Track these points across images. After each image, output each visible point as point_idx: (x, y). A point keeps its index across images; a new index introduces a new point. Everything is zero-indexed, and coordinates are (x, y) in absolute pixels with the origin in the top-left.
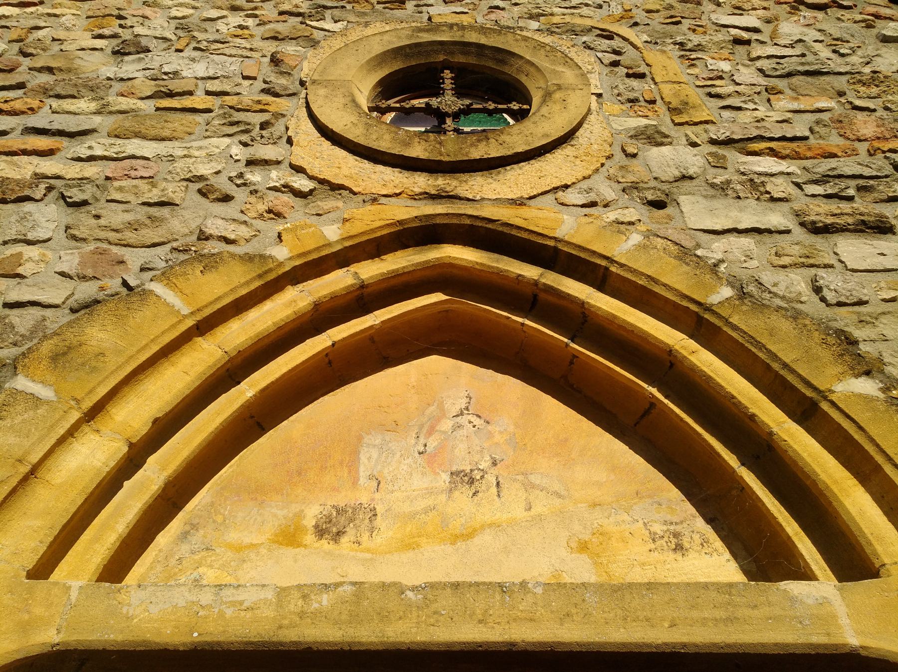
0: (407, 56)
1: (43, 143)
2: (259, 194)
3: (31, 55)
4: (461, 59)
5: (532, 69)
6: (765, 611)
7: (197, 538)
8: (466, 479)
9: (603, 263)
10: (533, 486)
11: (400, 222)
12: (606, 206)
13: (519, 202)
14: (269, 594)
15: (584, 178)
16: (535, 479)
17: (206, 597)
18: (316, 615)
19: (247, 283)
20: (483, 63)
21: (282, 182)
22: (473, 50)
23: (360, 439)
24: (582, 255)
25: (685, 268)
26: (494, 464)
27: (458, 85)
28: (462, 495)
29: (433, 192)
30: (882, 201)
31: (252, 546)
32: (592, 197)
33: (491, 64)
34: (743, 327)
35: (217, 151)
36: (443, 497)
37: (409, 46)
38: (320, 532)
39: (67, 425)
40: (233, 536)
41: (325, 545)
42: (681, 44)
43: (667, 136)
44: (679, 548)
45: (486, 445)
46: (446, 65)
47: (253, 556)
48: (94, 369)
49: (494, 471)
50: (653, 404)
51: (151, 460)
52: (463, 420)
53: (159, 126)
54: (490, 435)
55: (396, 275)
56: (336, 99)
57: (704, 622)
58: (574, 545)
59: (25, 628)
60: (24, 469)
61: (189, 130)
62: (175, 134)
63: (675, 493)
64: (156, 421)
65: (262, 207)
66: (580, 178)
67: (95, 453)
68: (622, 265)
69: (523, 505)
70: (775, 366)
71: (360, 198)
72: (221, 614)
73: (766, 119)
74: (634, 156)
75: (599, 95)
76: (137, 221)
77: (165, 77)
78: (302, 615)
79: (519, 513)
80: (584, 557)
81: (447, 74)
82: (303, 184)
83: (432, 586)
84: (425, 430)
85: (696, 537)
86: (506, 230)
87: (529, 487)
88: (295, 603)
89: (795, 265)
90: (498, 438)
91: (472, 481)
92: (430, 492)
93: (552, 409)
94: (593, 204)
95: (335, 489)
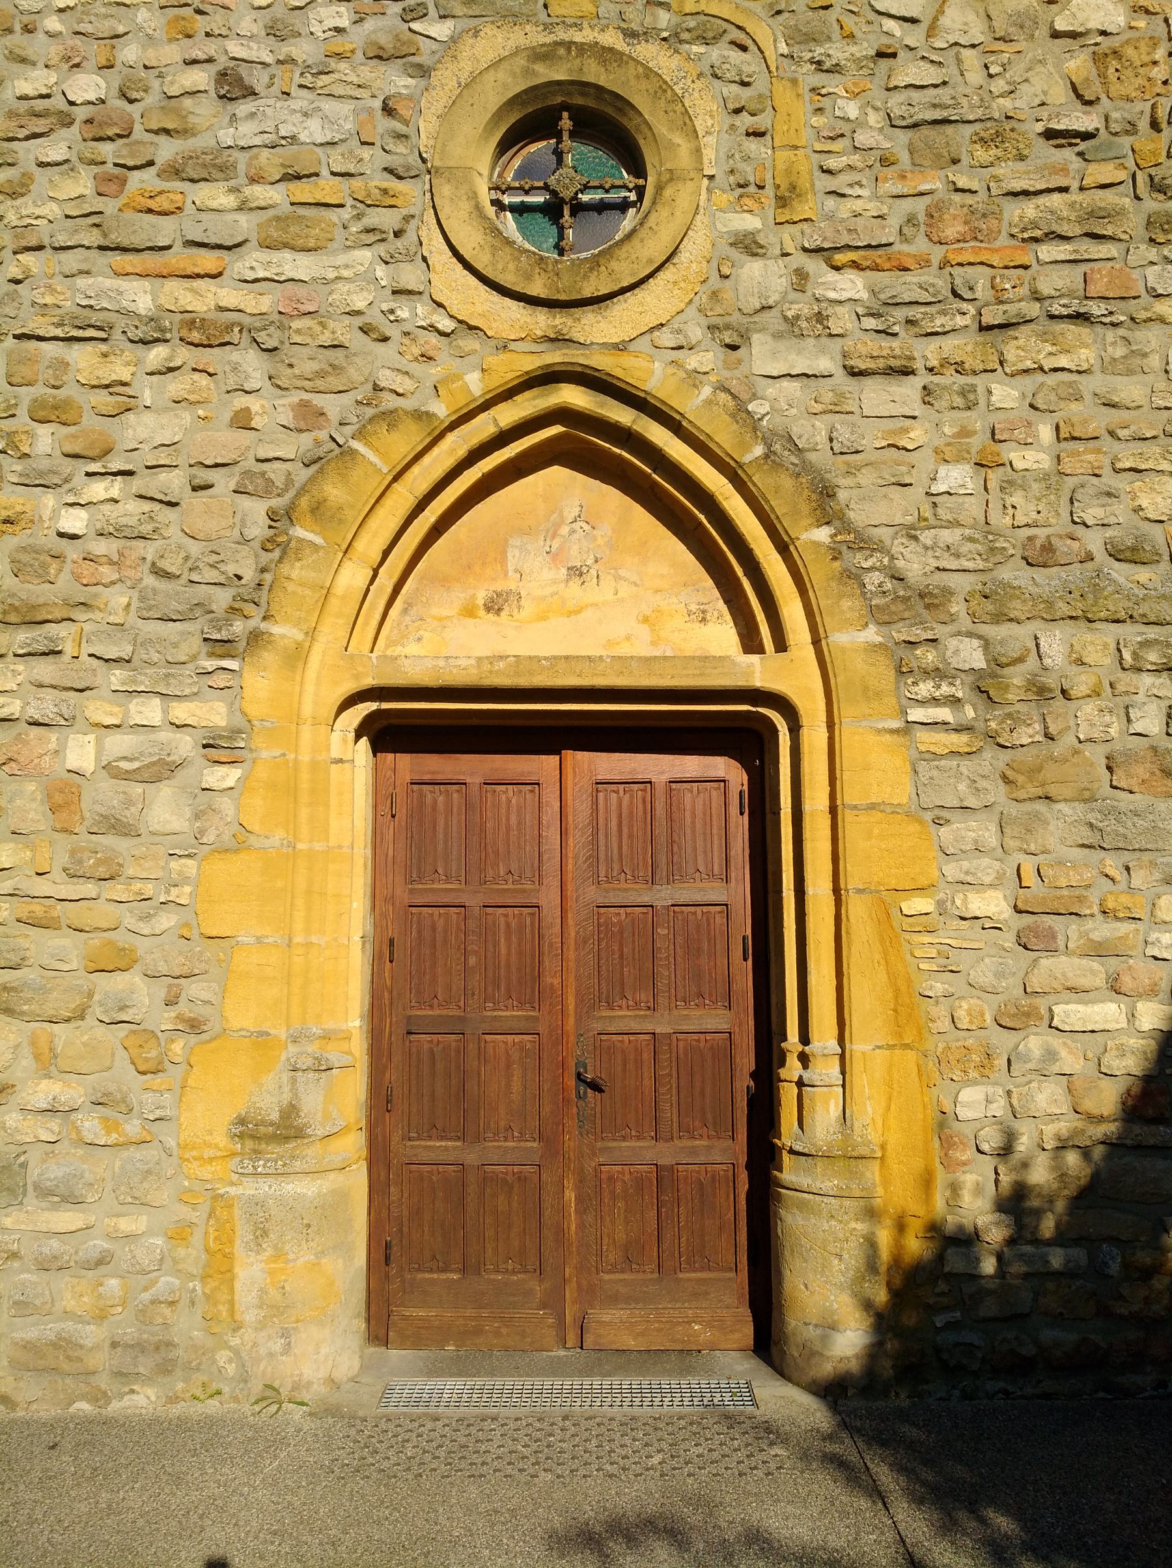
0: (524, 104)
1: (208, 261)
2: (412, 336)
3: (136, 100)
4: (579, 101)
5: (649, 134)
6: (720, 670)
7: (413, 612)
8: (577, 572)
9: (678, 417)
10: (620, 578)
13: (620, 347)
14: (473, 662)
16: (622, 572)
17: (442, 663)
18: (497, 672)
19: (422, 441)
20: (602, 108)
21: (428, 321)
22: (592, 91)
23: (506, 541)
24: (664, 408)
25: (735, 427)
26: (596, 561)
27: (579, 137)
28: (575, 583)
29: (552, 336)
31: (448, 618)
32: (681, 340)
33: (609, 110)
34: (760, 485)
35: (363, 269)
36: (563, 585)
37: (525, 92)
38: (488, 609)
40: (435, 611)
41: (491, 616)
42: (819, 63)
43: (762, 247)
44: (704, 620)
45: (591, 546)
46: (565, 107)
47: (449, 623)
48: (340, 521)
49: (596, 566)
50: (701, 524)
52: (576, 526)
54: (595, 539)
56: (461, 204)
57: (688, 676)
58: (640, 618)
61: (329, 236)
62: (319, 244)
63: (710, 583)
65: (416, 351)
68: (691, 422)
69: (612, 591)
70: (773, 516)
71: (493, 343)
72: (451, 672)
73: (864, 213)
74: (727, 277)
75: (711, 178)
76: (322, 370)
77: (283, 142)
78: (491, 672)
79: (610, 597)
80: (646, 626)
81: (565, 115)
82: (446, 324)
83: (555, 658)
84: (550, 534)
85: (716, 613)
86: (609, 379)
87: (618, 578)
88: (486, 667)
90: (600, 541)
91: (581, 575)
92: (554, 582)
93: (639, 512)
94: (680, 348)
95: (494, 579)
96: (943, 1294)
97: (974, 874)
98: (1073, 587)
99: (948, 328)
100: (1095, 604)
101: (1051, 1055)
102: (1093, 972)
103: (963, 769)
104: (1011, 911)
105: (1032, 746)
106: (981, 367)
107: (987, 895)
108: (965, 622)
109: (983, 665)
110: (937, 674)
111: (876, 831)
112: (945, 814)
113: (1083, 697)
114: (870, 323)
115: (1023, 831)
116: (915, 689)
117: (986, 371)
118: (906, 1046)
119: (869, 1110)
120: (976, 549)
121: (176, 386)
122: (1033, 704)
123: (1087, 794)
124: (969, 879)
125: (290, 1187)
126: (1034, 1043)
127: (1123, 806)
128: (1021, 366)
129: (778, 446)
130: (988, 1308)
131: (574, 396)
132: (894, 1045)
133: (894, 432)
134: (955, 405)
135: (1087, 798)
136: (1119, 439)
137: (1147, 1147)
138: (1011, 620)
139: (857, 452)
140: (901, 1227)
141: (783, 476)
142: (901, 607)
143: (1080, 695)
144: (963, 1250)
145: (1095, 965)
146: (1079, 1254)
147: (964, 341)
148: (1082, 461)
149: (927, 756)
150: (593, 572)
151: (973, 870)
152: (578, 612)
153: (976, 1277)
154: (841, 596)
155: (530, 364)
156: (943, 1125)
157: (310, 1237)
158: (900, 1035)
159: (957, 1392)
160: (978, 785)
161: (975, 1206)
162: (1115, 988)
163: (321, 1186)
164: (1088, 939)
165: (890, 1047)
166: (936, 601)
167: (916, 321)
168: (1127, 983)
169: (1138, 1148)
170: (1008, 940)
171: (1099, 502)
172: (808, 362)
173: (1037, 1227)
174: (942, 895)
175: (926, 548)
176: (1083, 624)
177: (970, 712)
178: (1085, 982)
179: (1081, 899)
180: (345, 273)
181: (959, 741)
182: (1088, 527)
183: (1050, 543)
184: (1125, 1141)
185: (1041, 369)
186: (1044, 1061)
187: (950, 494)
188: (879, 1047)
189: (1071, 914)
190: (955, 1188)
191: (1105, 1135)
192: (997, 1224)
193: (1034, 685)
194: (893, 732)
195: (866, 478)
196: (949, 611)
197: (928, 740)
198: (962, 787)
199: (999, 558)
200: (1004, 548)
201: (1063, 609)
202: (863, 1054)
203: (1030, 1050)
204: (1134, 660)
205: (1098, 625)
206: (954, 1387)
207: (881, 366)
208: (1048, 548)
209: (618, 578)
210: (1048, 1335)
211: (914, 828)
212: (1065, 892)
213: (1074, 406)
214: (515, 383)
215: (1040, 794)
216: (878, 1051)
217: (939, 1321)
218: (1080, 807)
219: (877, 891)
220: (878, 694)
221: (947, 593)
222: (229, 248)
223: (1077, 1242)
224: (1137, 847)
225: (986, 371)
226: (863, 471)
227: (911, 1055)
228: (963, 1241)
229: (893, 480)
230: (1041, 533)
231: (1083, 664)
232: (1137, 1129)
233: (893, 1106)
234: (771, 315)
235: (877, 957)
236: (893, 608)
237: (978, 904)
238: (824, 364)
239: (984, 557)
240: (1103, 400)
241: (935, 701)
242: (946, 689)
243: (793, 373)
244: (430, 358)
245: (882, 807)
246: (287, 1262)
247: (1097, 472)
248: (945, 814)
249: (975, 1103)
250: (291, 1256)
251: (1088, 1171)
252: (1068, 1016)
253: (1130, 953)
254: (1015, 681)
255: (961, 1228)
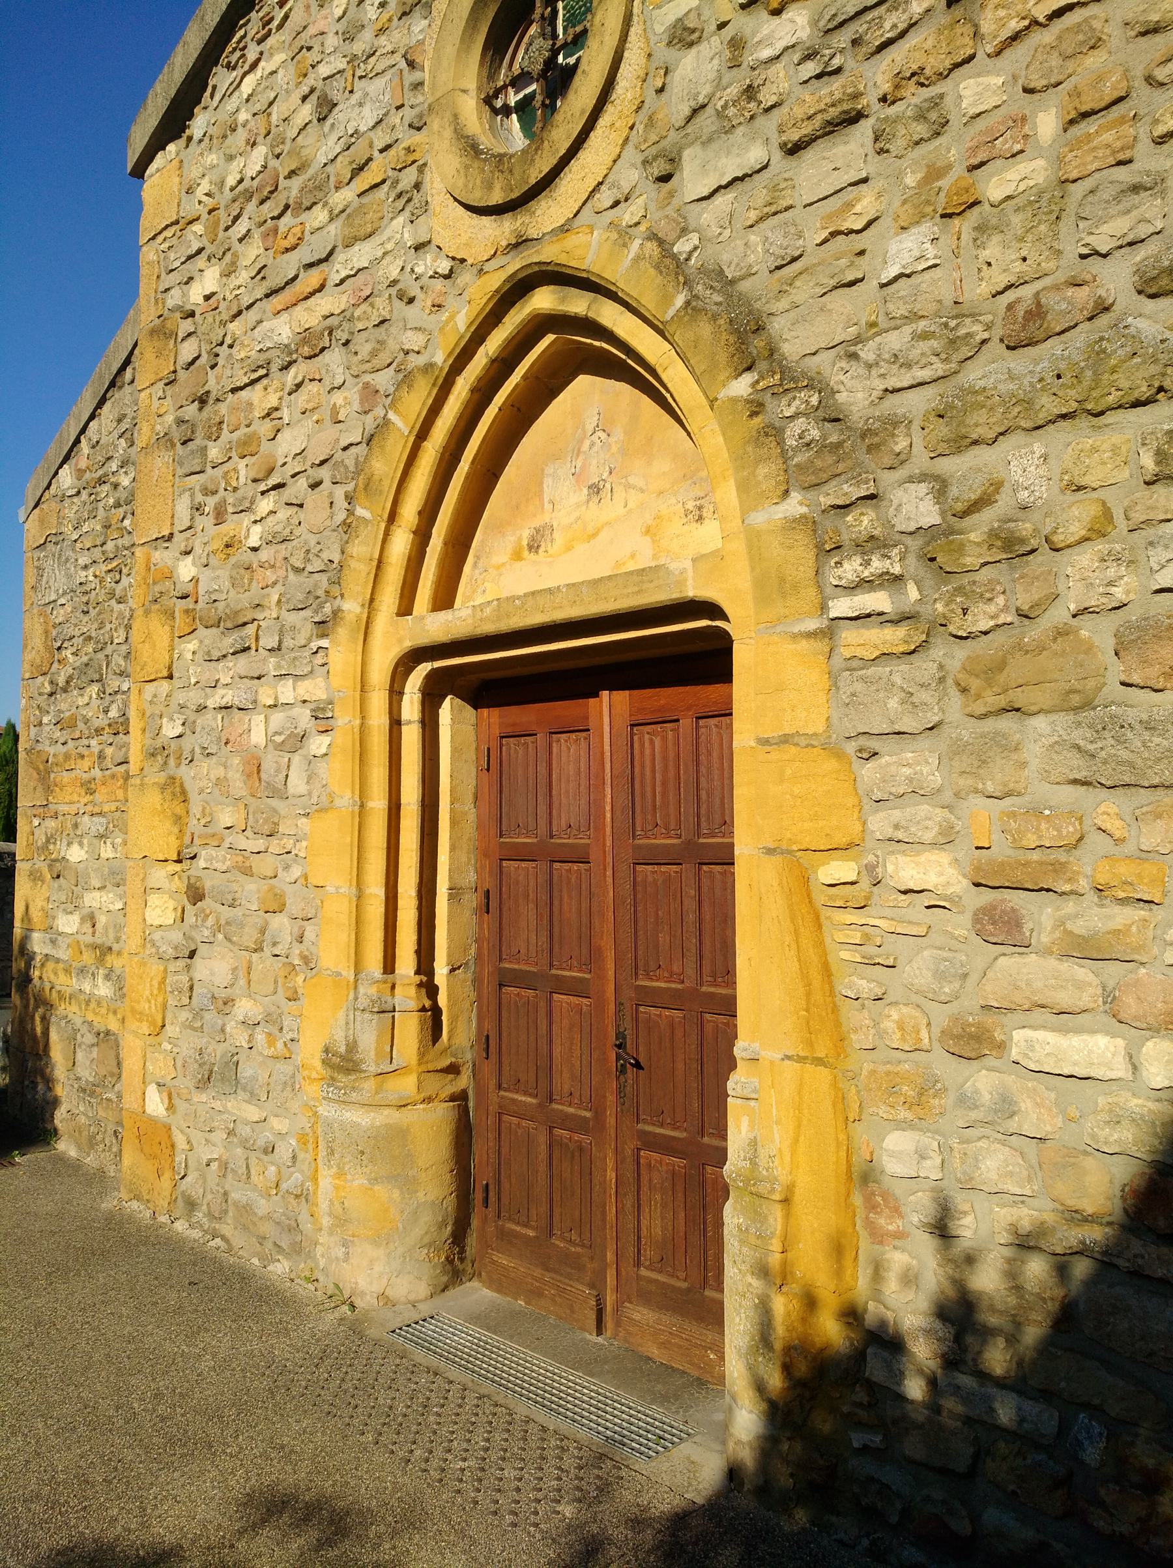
11: (497, 291)
12: (626, 200)
15: (615, 161)
16: (631, 480)
19: (429, 394)
23: (543, 470)
24: (603, 283)
30: (873, 54)
39: (382, 532)
41: (532, 556)
43: (693, 31)
51: (434, 531)
53: (71, 744)
55: (509, 342)
59: (400, 641)
60: (375, 563)
64: (420, 513)
66: (611, 163)
67: (401, 543)
77: (353, 140)
78: (481, 620)
79: (621, 511)
80: (648, 538)
89: (761, 219)
90: (614, 449)
96: (860, 1405)
97: (906, 828)
98: (1063, 366)
99: (902, 26)
100: (1097, 381)
101: (1006, 1107)
102: (1080, 986)
103: (897, 679)
104: (966, 883)
105: (999, 631)
106: (948, 64)
107: (922, 858)
108: (920, 460)
109: (937, 520)
110: (869, 545)
111: (789, 772)
112: (874, 744)
113: (1079, 543)
114: (811, 68)
115: (976, 763)
116: (839, 571)
117: (957, 66)
118: (819, 1062)
119: (777, 1136)
120: (932, 347)
121: (302, 399)
122: (1003, 566)
123: (1076, 699)
124: (900, 835)
125: (348, 1114)
126: (983, 1081)
127: (1132, 715)
128: (1006, 33)
129: (700, 287)
130: (913, 1447)
131: (543, 300)
132: (805, 1058)
133: (829, 217)
134: (916, 137)
135: (1078, 703)
136: (1162, 84)
137: (1149, 1278)
138: (975, 443)
139: (794, 259)
140: (810, 1302)
141: (702, 324)
142: (830, 459)
143: (1072, 540)
144: (886, 1354)
145: (1082, 972)
146: (1047, 1420)
147: (923, 36)
148: (1095, 149)
149: (855, 663)
150: (608, 486)
151: (903, 823)
152: (594, 535)
153: (901, 1398)
154: (758, 461)
155: (495, 281)
156: (864, 1177)
157: (364, 1163)
158: (810, 1044)
159: (865, 1542)
160: (914, 699)
161: (907, 1303)
162: (1114, 1011)
163: (374, 1118)
164: (1065, 930)
165: (801, 1059)
166: (876, 440)
167: (861, 37)
168: (1130, 1005)
169: (1136, 1274)
170: (960, 925)
171: (1120, 207)
172: (739, 160)
173: (979, 1353)
174: (871, 858)
175: (869, 366)
176: (1084, 422)
177: (913, 593)
178: (1064, 999)
179: (1059, 868)
180: (389, 246)
181: (894, 637)
182: (1105, 256)
183: (1039, 304)
184: (1115, 1261)
185: (1035, 22)
186: (996, 1111)
187: (908, 276)
188: (788, 1058)
189: (1041, 889)
190: (878, 1271)
191: (1083, 1243)
192: (927, 1332)
193: (998, 537)
194: (810, 635)
195: (804, 291)
196: (892, 450)
197: (854, 640)
198: (893, 703)
199: (966, 352)
200: (969, 335)
201: (1049, 406)
202: (772, 1062)
203: (977, 1092)
204: (1158, 463)
205: (1109, 418)
206: (868, 1535)
207: (817, 126)
208: (1037, 312)
209: (628, 486)
210: (992, 1516)
211: (832, 764)
212: (1035, 856)
213: (1094, 61)
214: (490, 306)
215: (1003, 704)
216: (787, 1062)
217: (857, 1439)
218: (1063, 720)
219: (790, 852)
220: (795, 587)
221: (893, 423)
222: (326, 259)
223: (1046, 1395)
224: (1156, 781)
225: (957, 66)
226: (798, 283)
227: (824, 1073)
228: (884, 1342)
229: (833, 282)
230: (1026, 292)
231: (1080, 488)
232: (1137, 1246)
233: (802, 1139)
234: (706, 115)
235: (788, 939)
236: (819, 463)
237: (906, 870)
238: (755, 155)
239: (943, 356)
240: (1138, 28)
241: (863, 585)
242: (878, 564)
243: (724, 183)
244: (439, 306)
245: (796, 740)
246: (346, 1181)
247: (1121, 156)
248: (874, 744)
249: (900, 1152)
250: (349, 1177)
251: (1059, 1292)
252: (1031, 1048)
253: (1136, 957)
254: (973, 536)
255: (883, 1324)
